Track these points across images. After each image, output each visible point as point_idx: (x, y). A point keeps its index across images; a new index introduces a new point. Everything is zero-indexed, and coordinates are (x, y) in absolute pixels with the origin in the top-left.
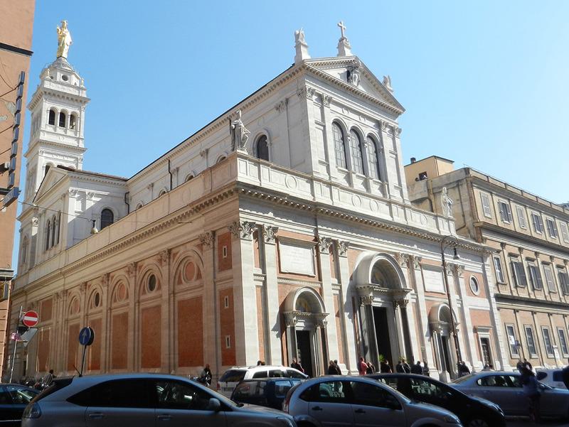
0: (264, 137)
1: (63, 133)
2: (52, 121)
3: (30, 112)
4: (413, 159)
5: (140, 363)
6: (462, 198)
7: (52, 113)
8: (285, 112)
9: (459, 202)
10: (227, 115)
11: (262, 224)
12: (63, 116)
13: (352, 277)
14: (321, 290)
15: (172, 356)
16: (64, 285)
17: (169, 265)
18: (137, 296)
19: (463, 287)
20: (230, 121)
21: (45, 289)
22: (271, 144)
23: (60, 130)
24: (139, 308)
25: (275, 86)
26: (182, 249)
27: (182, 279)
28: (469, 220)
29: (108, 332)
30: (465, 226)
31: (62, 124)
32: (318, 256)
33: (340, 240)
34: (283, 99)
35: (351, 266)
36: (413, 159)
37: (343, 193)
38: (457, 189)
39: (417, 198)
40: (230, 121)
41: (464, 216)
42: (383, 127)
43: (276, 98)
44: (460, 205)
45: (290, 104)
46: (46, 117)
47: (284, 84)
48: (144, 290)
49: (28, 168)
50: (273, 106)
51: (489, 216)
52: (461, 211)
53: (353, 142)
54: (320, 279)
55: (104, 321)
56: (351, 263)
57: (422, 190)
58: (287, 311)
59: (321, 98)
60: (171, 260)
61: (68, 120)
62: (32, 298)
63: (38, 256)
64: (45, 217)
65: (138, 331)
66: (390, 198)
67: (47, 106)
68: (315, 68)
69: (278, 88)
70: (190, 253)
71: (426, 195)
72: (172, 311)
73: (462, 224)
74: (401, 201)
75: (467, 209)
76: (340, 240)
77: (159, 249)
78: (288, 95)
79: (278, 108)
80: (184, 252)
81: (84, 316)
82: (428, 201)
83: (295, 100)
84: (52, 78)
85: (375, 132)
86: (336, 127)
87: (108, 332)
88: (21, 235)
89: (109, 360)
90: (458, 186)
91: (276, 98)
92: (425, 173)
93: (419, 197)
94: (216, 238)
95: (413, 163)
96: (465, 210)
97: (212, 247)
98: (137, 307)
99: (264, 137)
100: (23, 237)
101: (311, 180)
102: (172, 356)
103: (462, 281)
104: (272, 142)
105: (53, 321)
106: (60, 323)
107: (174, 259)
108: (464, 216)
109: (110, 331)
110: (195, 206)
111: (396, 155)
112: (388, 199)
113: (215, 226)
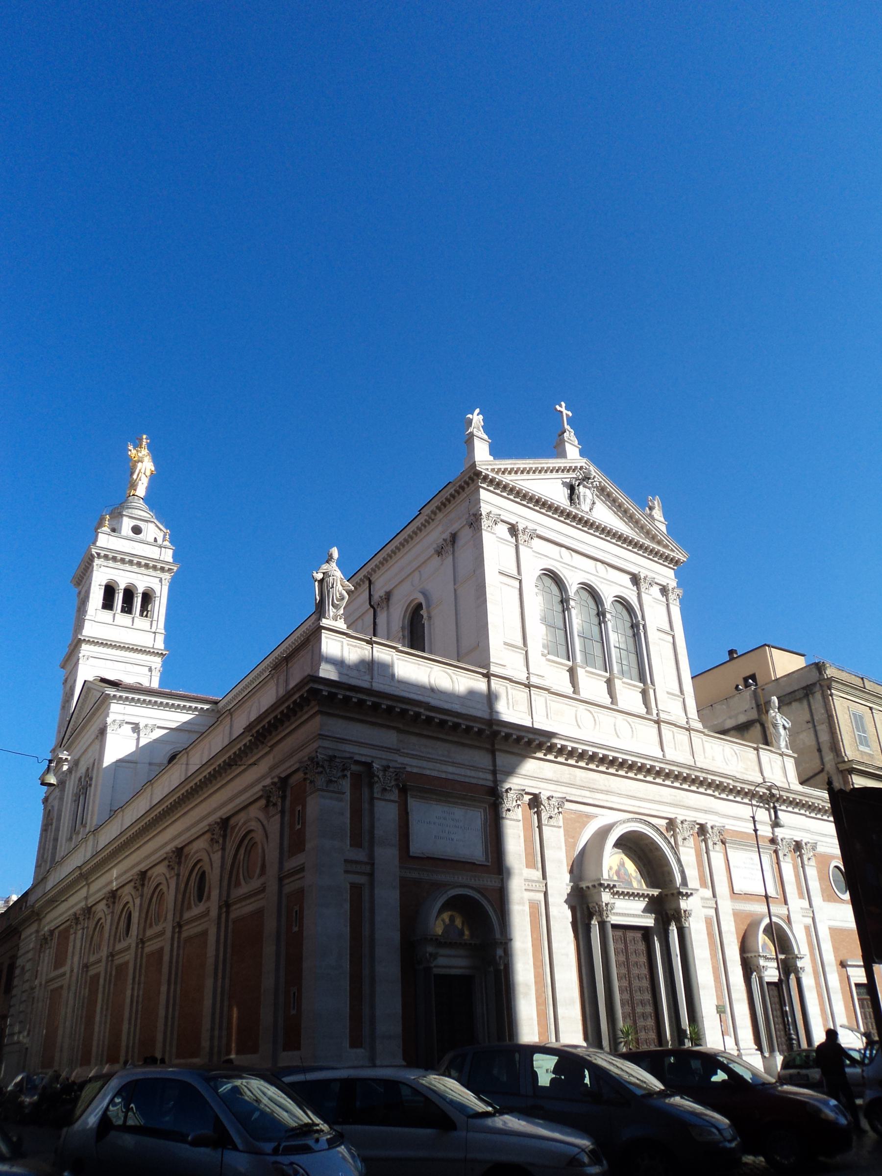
0: (419, 606)
1: (111, 621)
2: (108, 604)
3: (77, 590)
4: (731, 652)
5: (174, 1050)
6: (816, 718)
7: (110, 591)
8: (451, 557)
9: (810, 725)
10: (364, 572)
11: (369, 760)
12: (129, 594)
13: (572, 866)
14: (789, 917)
15: (216, 1033)
16: (86, 898)
17: (223, 849)
18: (178, 915)
19: (815, 885)
20: (370, 583)
21: (63, 907)
22: (430, 618)
23: (124, 619)
24: (179, 938)
25: (434, 513)
26: (242, 817)
27: (241, 877)
28: (829, 757)
29: (136, 986)
30: (822, 770)
31: (127, 608)
32: (778, 863)
33: (680, 818)
34: (447, 535)
35: (570, 843)
36: (731, 652)
37: (557, 704)
38: (805, 703)
39: (740, 722)
40: (370, 583)
41: (819, 750)
42: (643, 586)
43: (436, 535)
44: (812, 729)
45: (460, 542)
46: (96, 596)
47: (450, 507)
48: (189, 903)
49: (65, 687)
50: (431, 551)
51: (867, 750)
52: (814, 743)
53: (579, 618)
54: (786, 903)
55: (131, 966)
56: (571, 835)
57: (747, 707)
58: (749, 952)
59: (513, 530)
60: (228, 838)
61: (138, 602)
62: (51, 921)
63: (61, 846)
64: (76, 771)
65: (176, 983)
66: (657, 714)
67: (101, 576)
68: (499, 477)
69: (440, 516)
70: (253, 825)
71: (753, 715)
72: (222, 940)
73: (816, 765)
74: (683, 722)
75: (824, 737)
76: (680, 818)
77: (211, 819)
78: (455, 527)
79: (439, 552)
80: (245, 823)
81: (108, 957)
82: (758, 725)
83: (465, 535)
84: (114, 530)
85: (631, 596)
86: (548, 582)
87: (136, 986)
88: (45, 809)
89: (134, 1043)
90: (807, 696)
91: (436, 535)
92: (753, 677)
93: (742, 719)
94: (288, 793)
95: (732, 659)
96: (821, 740)
97: (279, 809)
98: (176, 935)
99: (419, 606)
100: (47, 811)
101: (487, 676)
102: (216, 1033)
103: (812, 872)
104: (433, 614)
105: (66, 968)
106: (75, 971)
107: (231, 835)
108: (819, 750)
109: (139, 984)
110: (254, 731)
111: (673, 637)
112: (655, 717)
113: (283, 771)
